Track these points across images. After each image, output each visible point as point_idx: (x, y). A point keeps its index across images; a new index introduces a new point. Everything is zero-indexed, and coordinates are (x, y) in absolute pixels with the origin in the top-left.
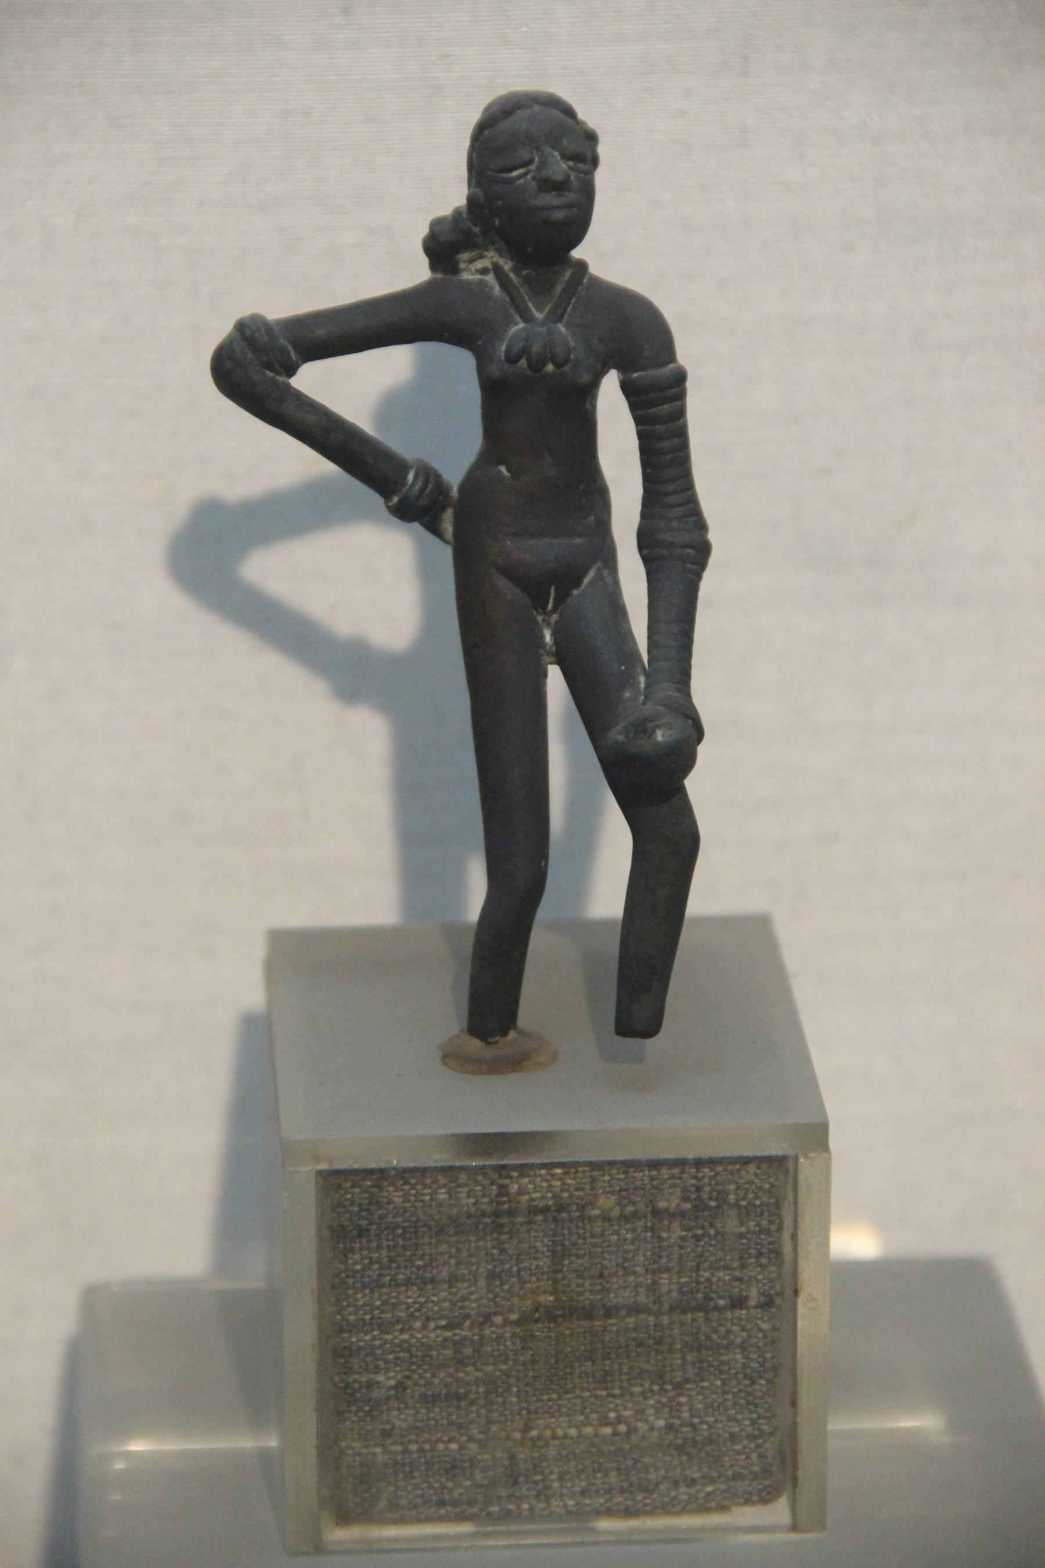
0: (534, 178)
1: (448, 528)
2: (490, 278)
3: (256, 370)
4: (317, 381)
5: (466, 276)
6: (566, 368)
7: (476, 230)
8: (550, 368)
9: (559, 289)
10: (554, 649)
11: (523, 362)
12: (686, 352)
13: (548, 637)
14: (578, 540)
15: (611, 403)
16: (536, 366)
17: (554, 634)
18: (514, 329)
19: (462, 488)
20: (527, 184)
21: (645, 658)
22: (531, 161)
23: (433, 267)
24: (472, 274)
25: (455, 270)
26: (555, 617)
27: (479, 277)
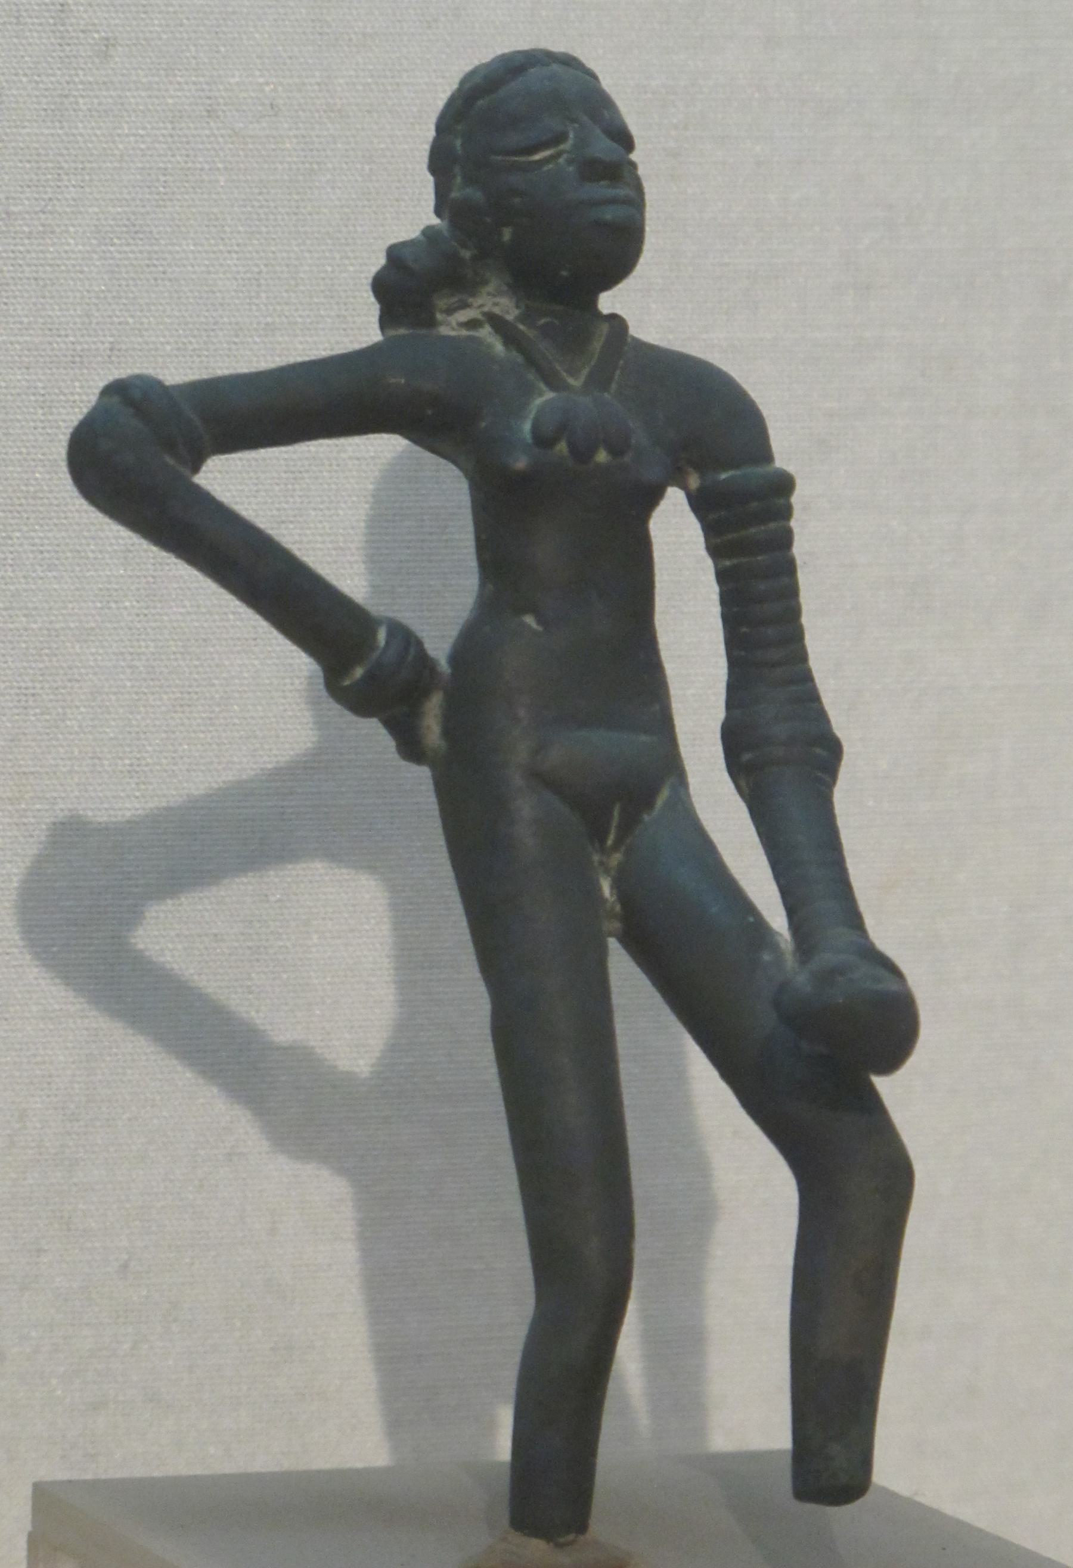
0: (570, 162)
1: (432, 728)
2: (486, 333)
3: (143, 459)
4: (234, 479)
5: (444, 331)
6: (627, 459)
7: (466, 254)
8: (602, 456)
9: (597, 345)
10: (618, 908)
11: (562, 447)
12: (786, 450)
13: (606, 887)
14: (644, 738)
15: (676, 532)
16: (582, 453)
17: (616, 885)
18: (538, 401)
19: (456, 658)
20: (531, 191)
21: (777, 919)
22: (559, 138)
23: (385, 321)
24: (453, 329)
25: (432, 323)
26: (616, 858)
27: (464, 332)
